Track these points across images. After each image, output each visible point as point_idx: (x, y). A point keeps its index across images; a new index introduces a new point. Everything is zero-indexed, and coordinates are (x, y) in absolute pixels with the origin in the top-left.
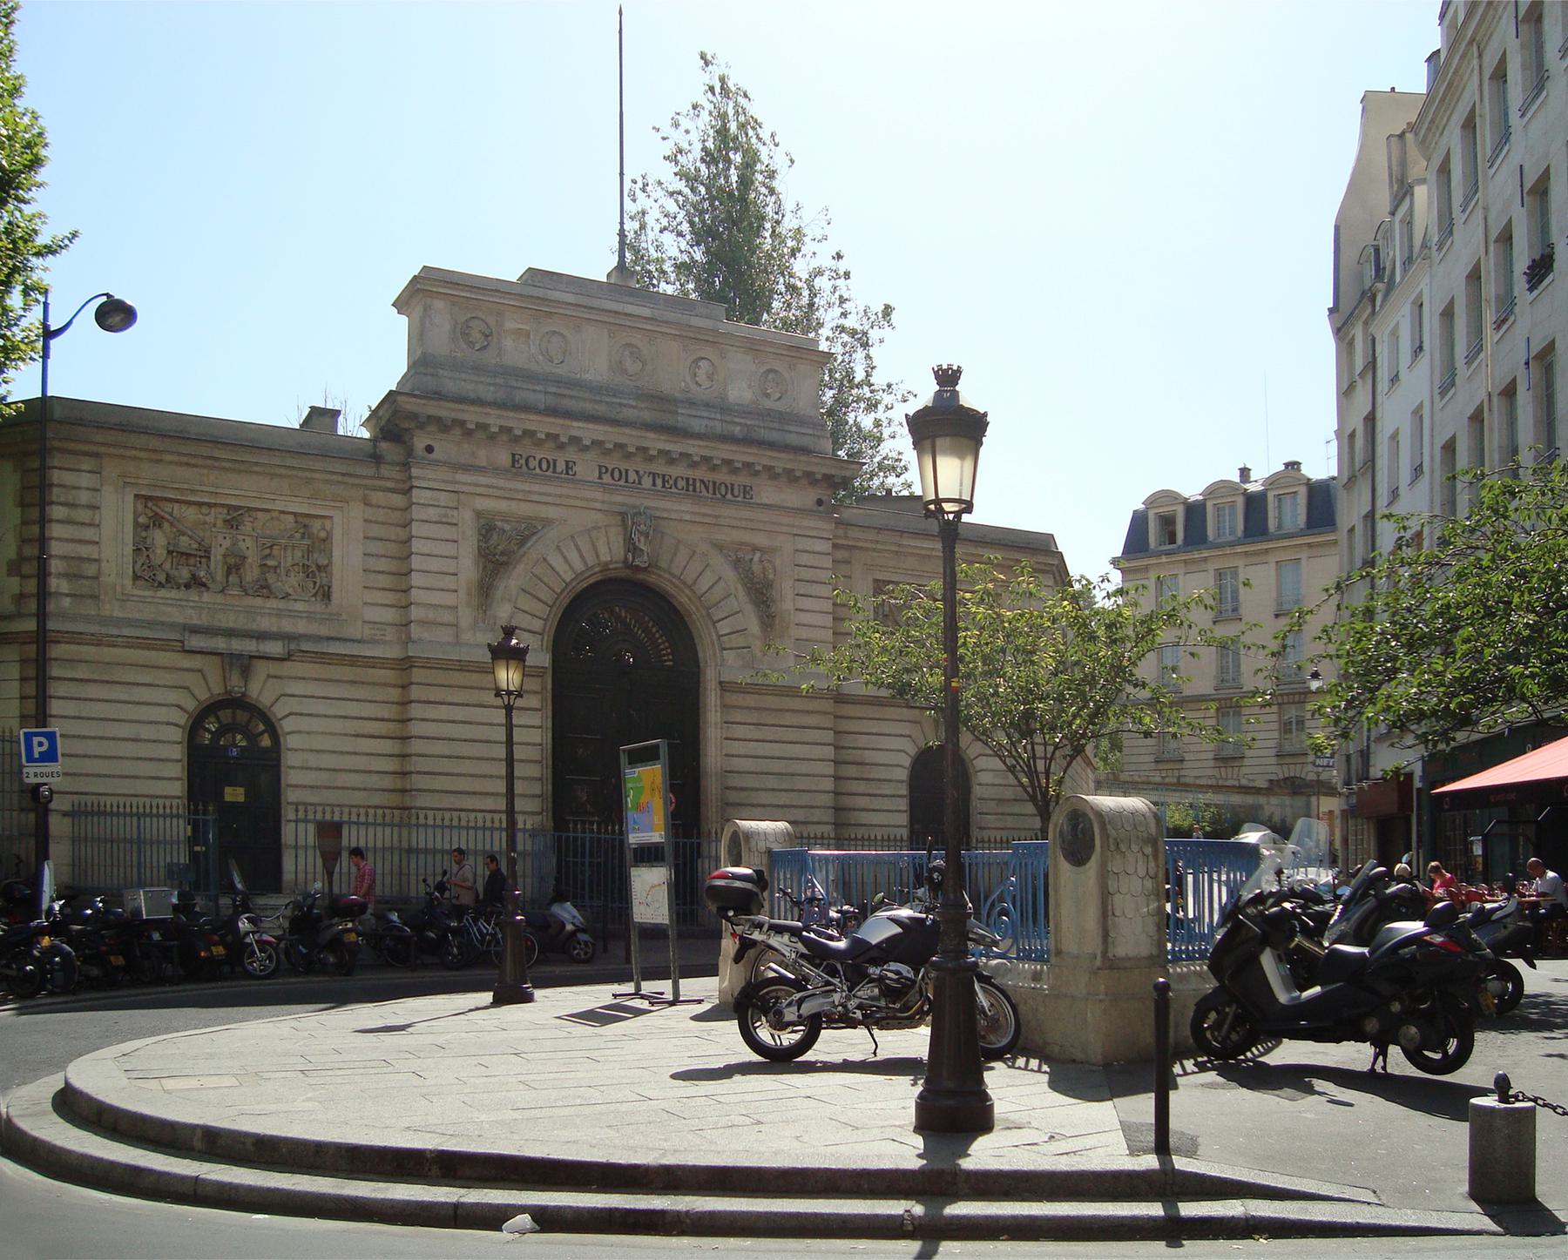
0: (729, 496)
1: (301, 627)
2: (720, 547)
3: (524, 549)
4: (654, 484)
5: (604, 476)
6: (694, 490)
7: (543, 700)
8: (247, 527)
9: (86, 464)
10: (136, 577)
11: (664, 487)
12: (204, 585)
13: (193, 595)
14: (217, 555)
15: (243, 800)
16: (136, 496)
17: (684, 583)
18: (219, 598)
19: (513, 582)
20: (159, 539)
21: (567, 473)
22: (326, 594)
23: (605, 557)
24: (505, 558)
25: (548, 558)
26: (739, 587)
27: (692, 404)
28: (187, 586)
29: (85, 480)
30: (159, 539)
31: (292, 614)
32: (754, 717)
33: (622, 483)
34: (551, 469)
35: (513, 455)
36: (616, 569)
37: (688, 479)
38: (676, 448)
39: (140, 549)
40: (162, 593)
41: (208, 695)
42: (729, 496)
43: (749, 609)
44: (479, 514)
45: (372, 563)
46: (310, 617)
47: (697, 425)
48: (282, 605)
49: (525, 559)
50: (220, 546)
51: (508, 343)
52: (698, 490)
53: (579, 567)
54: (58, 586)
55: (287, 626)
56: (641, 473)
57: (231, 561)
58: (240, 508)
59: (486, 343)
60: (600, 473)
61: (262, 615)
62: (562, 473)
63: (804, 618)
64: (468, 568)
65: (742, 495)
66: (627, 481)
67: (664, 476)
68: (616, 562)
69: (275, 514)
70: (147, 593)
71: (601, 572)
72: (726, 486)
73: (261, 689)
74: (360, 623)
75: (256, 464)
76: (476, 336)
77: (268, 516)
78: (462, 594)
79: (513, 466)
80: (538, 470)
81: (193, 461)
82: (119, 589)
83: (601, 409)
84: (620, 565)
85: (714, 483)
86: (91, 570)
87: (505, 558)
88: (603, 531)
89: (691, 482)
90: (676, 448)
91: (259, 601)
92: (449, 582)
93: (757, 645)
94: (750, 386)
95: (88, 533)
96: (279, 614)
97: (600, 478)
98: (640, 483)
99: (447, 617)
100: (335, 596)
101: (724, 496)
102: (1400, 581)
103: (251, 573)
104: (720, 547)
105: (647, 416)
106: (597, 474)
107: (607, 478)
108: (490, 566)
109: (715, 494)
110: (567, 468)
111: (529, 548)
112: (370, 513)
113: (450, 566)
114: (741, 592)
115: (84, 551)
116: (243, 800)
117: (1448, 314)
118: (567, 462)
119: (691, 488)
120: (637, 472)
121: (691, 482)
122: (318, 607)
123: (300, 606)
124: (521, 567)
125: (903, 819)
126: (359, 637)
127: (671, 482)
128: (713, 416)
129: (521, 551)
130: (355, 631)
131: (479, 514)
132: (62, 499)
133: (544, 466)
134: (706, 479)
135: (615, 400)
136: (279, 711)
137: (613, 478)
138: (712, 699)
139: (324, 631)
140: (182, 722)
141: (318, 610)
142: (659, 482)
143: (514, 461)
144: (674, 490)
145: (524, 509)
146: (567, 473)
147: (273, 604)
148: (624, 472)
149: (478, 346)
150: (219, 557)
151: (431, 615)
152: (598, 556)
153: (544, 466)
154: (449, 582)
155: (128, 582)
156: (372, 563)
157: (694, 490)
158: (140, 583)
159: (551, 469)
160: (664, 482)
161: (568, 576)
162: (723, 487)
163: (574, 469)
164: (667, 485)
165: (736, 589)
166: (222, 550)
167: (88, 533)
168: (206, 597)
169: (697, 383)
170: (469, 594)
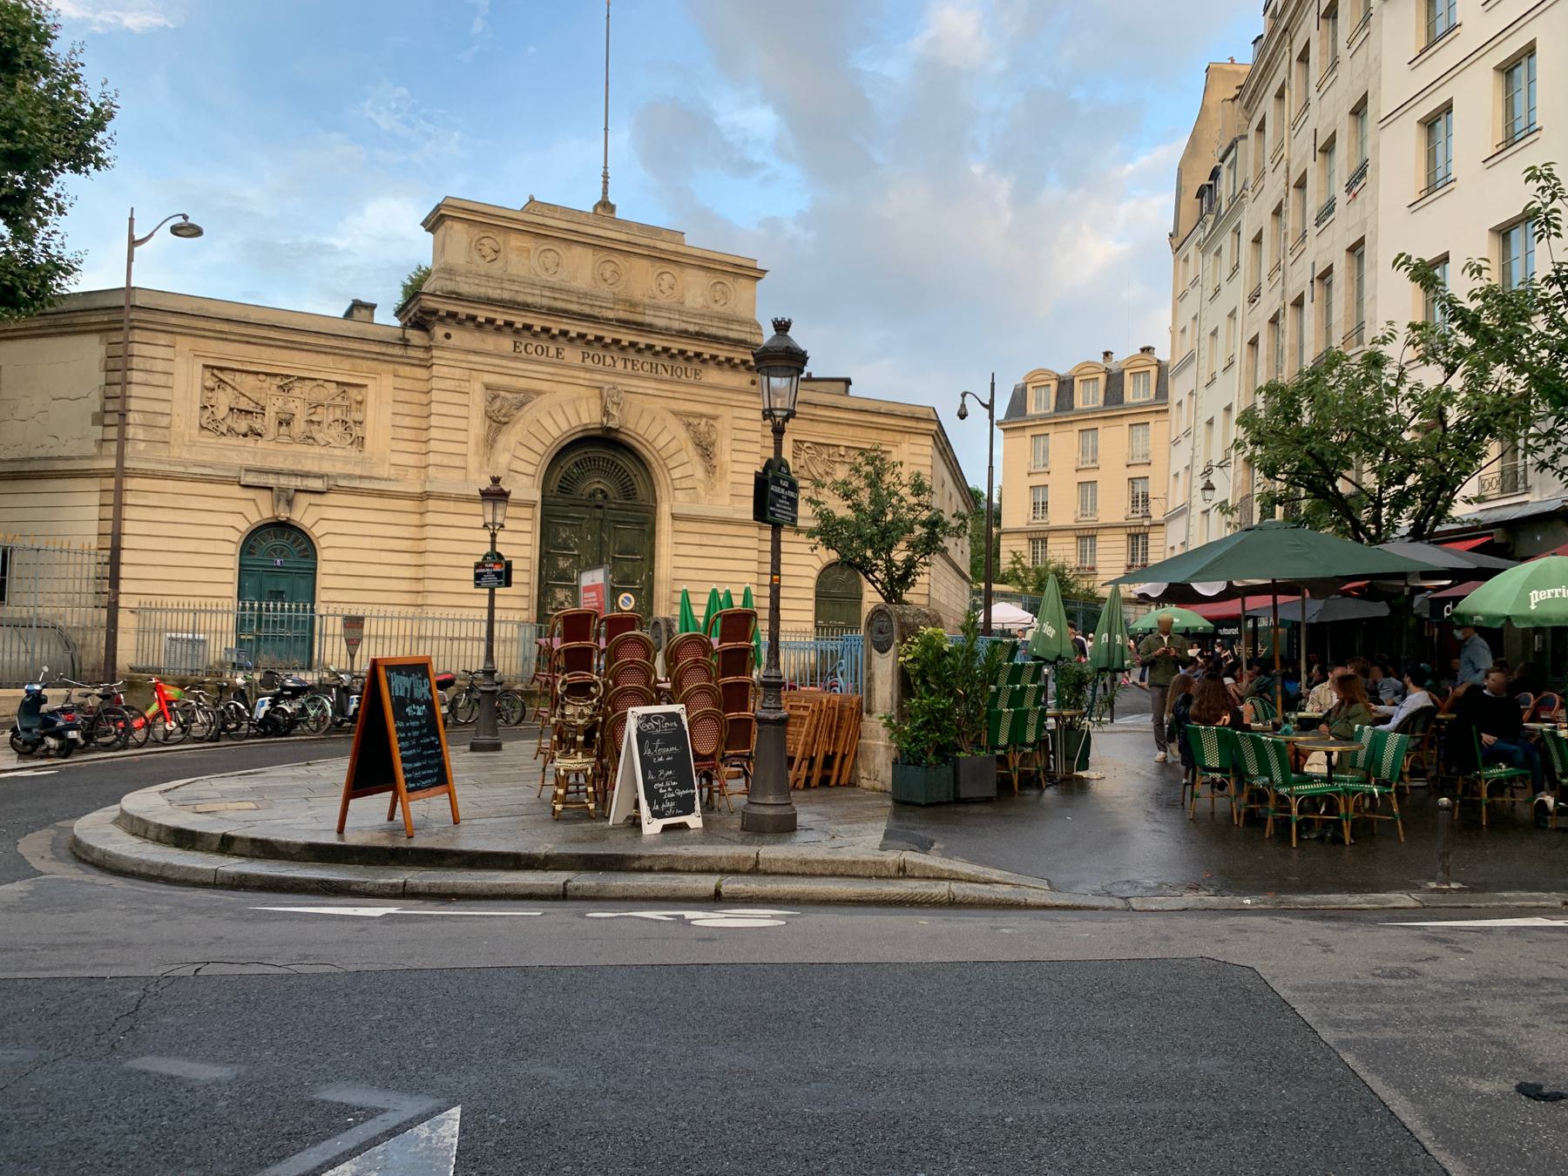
0: (684, 377)
1: (339, 468)
2: (675, 413)
7: (534, 526)
8: (296, 392)
9: (163, 339)
10: (202, 427)
12: (260, 435)
13: (250, 441)
14: (271, 412)
16: (206, 366)
18: (272, 445)
19: (510, 438)
20: (224, 399)
22: (360, 442)
23: (585, 420)
27: (657, 308)
28: (245, 435)
29: (161, 352)
30: (224, 399)
31: (332, 458)
32: (696, 539)
33: (601, 365)
38: (642, 341)
39: (205, 407)
40: (223, 440)
41: (259, 519)
43: (696, 459)
44: (487, 387)
45: (399, 420)
46: (347, 460)
47: (660, 322)
48: (323, 451)
50: (275, 404)
51: (513, 257)
53: (565, 427)
54: (135, 433)
55: (326, 468)
57: (283, 416)
58: (288, 376)
61: (306, 458)
63: (737, 467)
64: (477, 426)
69: (321, 382)
70: (210, 440)
73: (304, 515)
74: (387, 465)
75: (305, 344)
76: (487, 250)
77: (314, 383)
78: (472, 444)
81: (253, 340)
82: (187, 437)
83: (587, 310)
86: (164, 421)
90: (642, 341)
91: (304, 448)
92: (460, 436)
93: (701, 488)
95: (163, 393)
96: (321, 457)
99: (458, 461)
100: (367, 442)
103: (299, 426)
104: (675, 413)
105: (623, 315)
107: (588, 362)
108: (494, 425)
112: (398, 382)
113: (462, 424)
114: (691, 447)
115: (158, 407)
122: (353, 452)
123: (337, 452)
124: (519, 426)
125: (811, 616)
126: (386, 476)
129: (519, 414)
130: (383, 471)
131: (487, 387)
132: (141, 367)
133: (539, 350)
136: (316, 532)
138: (664, 526)
139: (358, 472)
140: (236, 540)
141: (353, 454)
142: (629, 365)
145: (522, 383)
147: (316, 449)
149: (488, 259)
150: (273, 414)
151: (446, 461)
153: (539, 350)
154: (460, 436)
155: (195, 431)
156: (399, 420)
158: (206, 433)
161: (556, 434)
166: (276, 409)
167: (163, 393)
168: (261, 443)
170: (477, 444)
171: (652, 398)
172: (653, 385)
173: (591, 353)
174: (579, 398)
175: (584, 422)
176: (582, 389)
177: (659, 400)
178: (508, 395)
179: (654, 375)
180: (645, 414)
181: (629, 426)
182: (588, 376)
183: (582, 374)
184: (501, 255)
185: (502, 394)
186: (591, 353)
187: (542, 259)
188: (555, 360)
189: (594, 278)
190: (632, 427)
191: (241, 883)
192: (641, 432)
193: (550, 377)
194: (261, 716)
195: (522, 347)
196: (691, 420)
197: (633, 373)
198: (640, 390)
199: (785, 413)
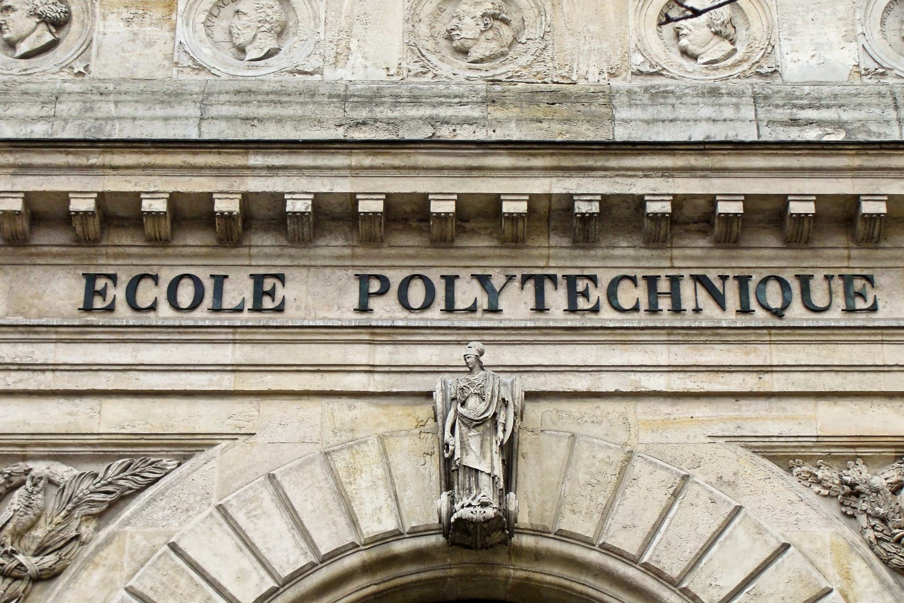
0: (797, 313)
3: (112, 527)
4: (540, 307)
5: (373, 303)
6: (677, 309)
11: (572, 309)
15: (288, 209)
17: (658, 575)
21: (257, 308)
24: (50, 560)
25: (182, 545)
26: (859, 568)
34: (208, 301)
35: (91, 279)
36: (418, 556)
37: (652, 282)
42: (797, 313)
49: (110, 553)
52: (688, 304)
56: (497, 281)
59: (48, 38)
60: (365, 295)
62: (238, 310)
65: (840, 301)
66: (450, 308)
67: (571, 281)
68: (415, 533)
71: (367, 569)
72: (784, 285)
79: (88, 308)
80: (165, 311)
84: (437, 540)
85: (743, 281)
87: (50, 560)
88: (372, 449)
89: (664, 286)
94: (849, 37)
97: (363, 308)
98: (494, 310)
101: (778, 313)
102: (880, 507)
106: (353, 299)
109: (745, 310)
110: (259, 294)
111: (127, 522)
116: (288, 209)
117: (63, 539)
118: (258, 280)
119: (665, 304)
120: (483, 280)
121: (664, 286)
127: (598, 294)
128: (728, 113)
129: (103, 534)
134: (712, 275)
135: (413, 112)
137: (407, 307)
142: (557, 298)
143: (91, 292)
144: (608, 316)
146: (257, 308)
148: (209, 285)
152: (354, 523)
153: (186, 295)
157: (677, 309)
159: (208, 301)
160: (573, 295)
162: (773, 289)
163: (280, 292)
164: (582, 303)
165: (847, 576)
169: (684, 52)
171: (664, 408)
172: (662, 355)
173: (396, 277)
174: (353, 445)
175: (372, 527)
176: (362, 407)
177: (702, 410)
178: (63, 472)
179: (666, 318)
180: (638, 467)
181: (569, 523)
182: (382, 355)
183: (359, 354)
184: (73, 35)
185: (39, 468)
186: (396, 277)
187: (220, 27)
188: (247, 317)
189: (412, 47)
190: (585, 527)
191: (569, 538)
192: (629, 543)
193: (227, 382)
194: (805, 222)
195: (119, 293)
196: (857, 473)
197: (574, 320)
198: (608, 383)
199: (872, 66)
